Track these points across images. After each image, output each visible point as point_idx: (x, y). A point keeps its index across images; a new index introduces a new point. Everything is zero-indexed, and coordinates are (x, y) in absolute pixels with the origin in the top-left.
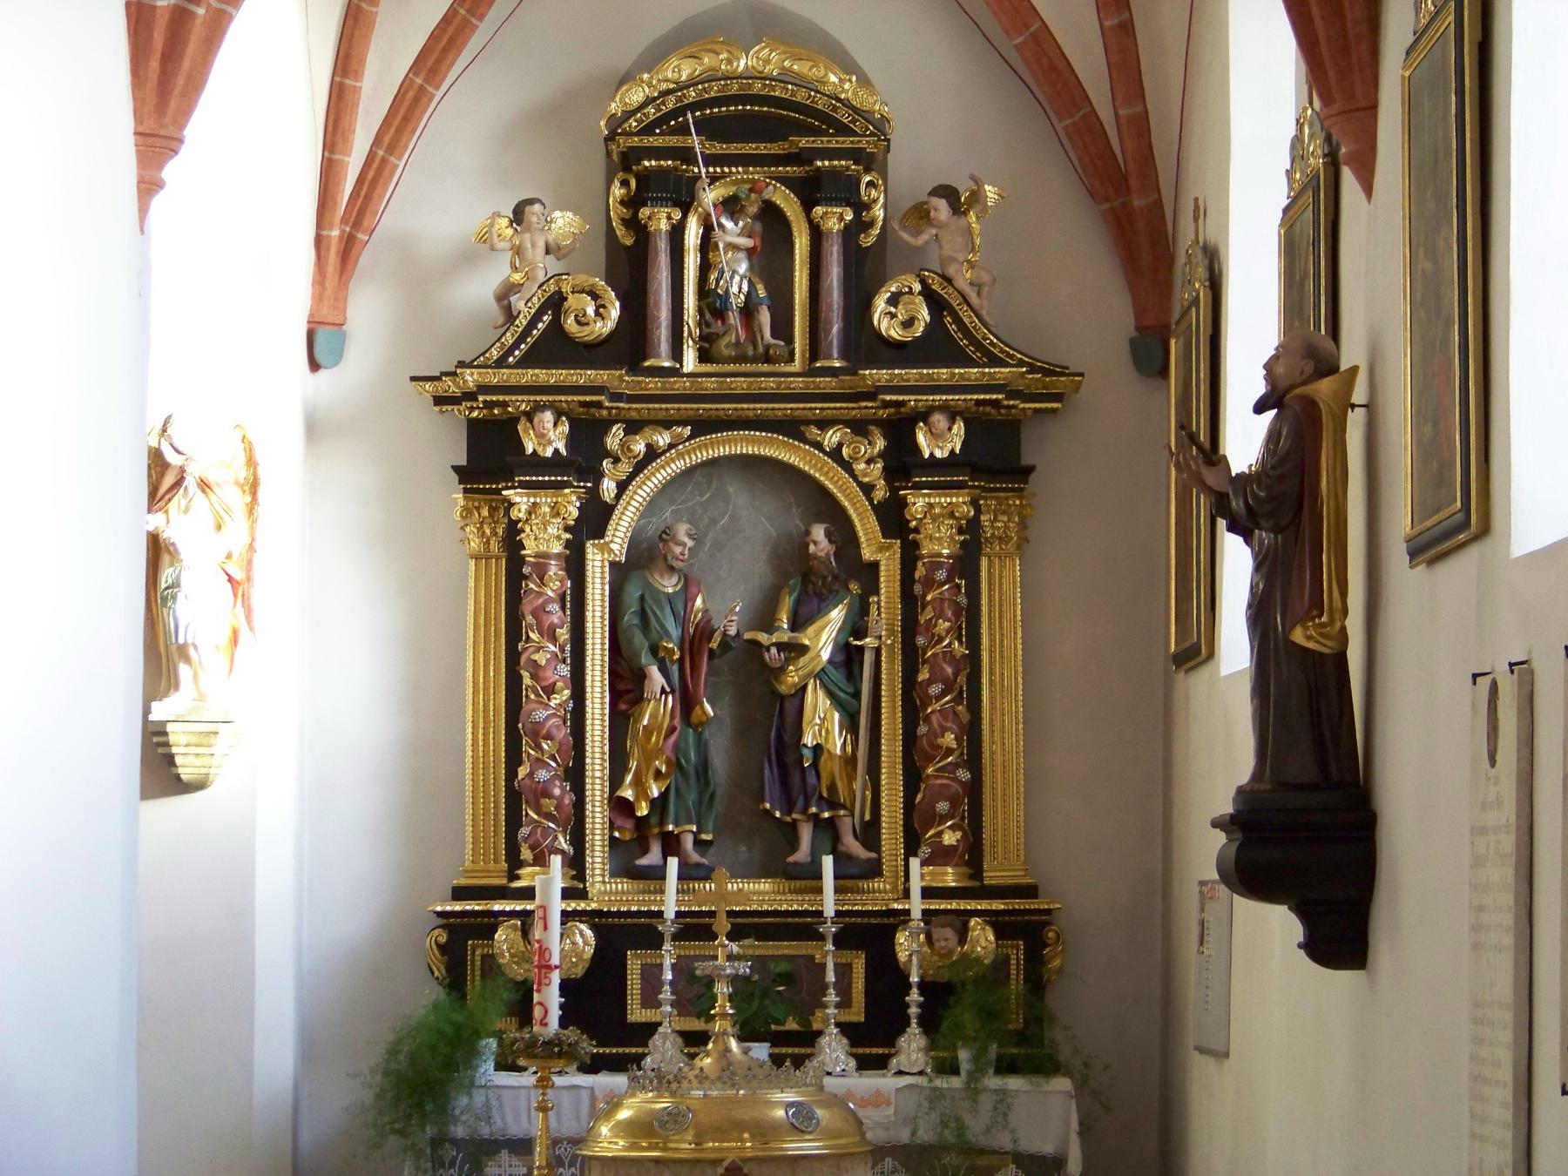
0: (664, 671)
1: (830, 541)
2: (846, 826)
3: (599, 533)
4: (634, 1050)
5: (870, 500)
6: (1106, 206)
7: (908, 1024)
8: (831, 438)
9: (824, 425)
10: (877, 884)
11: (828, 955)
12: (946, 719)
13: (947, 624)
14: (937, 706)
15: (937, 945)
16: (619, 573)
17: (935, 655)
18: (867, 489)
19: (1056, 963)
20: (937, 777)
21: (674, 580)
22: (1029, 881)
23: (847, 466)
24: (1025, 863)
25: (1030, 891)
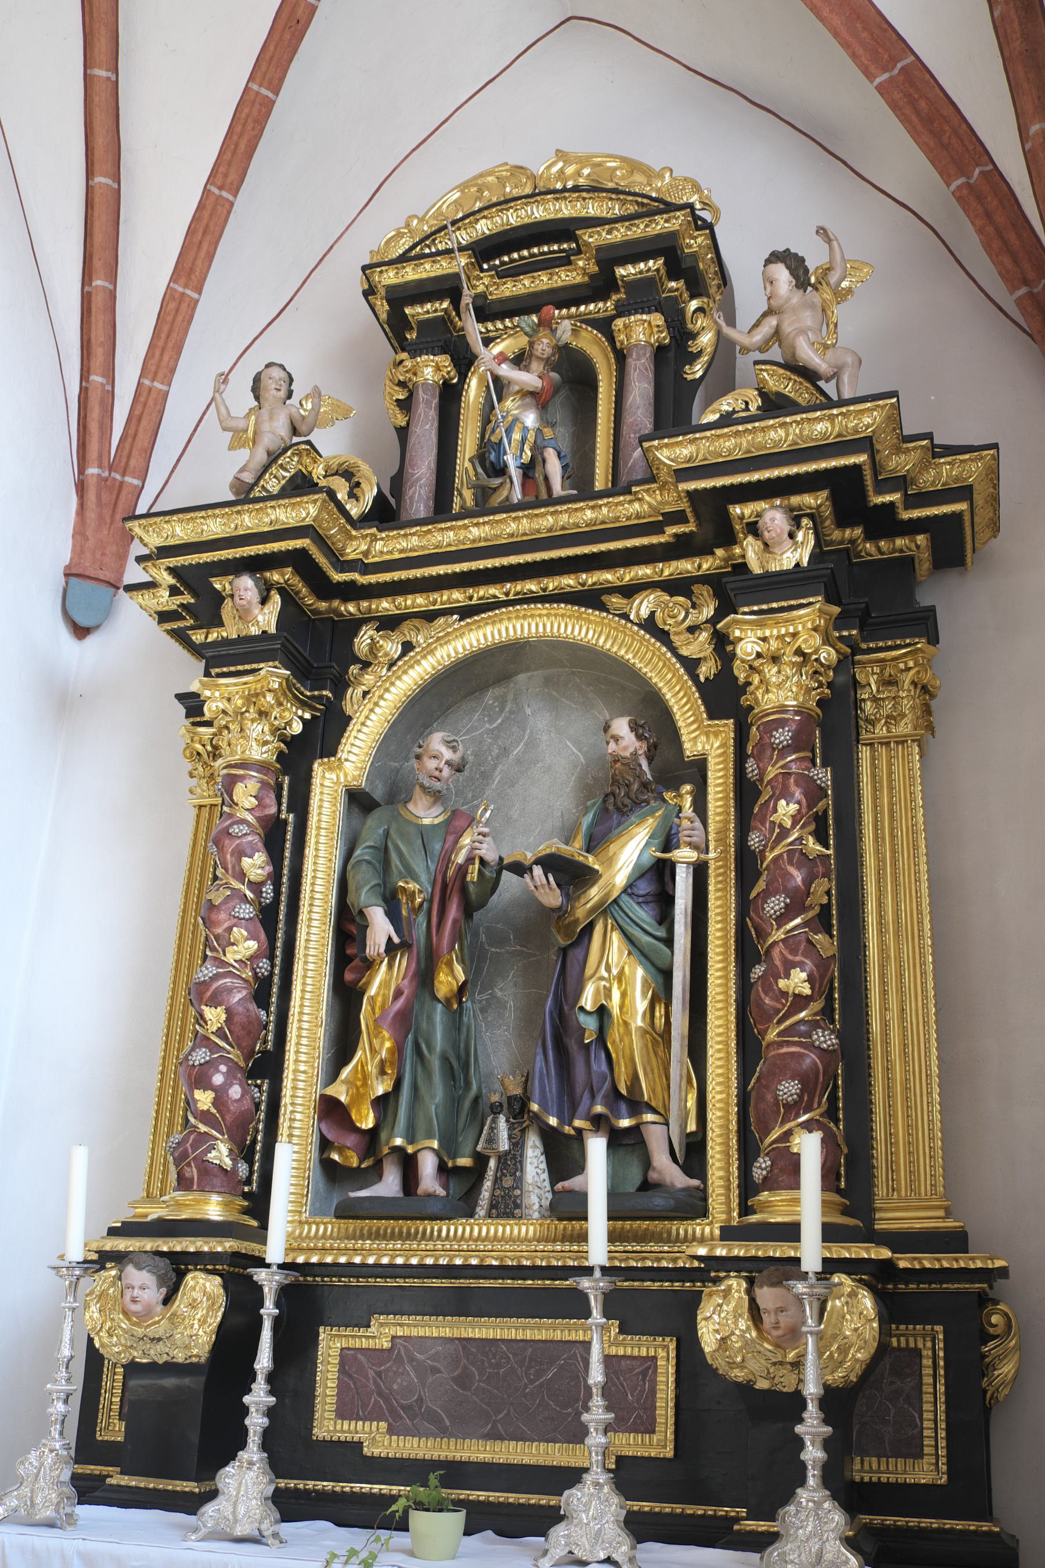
0: (393, 915)
1: (639, 737)
2: (656, 1139)
3: (329, 749)
4: (376, 1488)
5: (695, 678)
6: (1023, 290)
7: (242, 1445)
8: (644, 606)
9: (629, 591)
10: (698, 1228)
11: (599, 1338)
12: (794, 951)
13: (793, 808)
14: (779, 935)
15: (768, 1320)
16: (358, 801)
17: (776, 859)
18: (691, 665)
19: (1006, 1369)
20: (781, 1044)
21: (437, 810)
22: (950, 1223)
23: (663, 636)
24: (946, 1196)
25: (956, 1241)
